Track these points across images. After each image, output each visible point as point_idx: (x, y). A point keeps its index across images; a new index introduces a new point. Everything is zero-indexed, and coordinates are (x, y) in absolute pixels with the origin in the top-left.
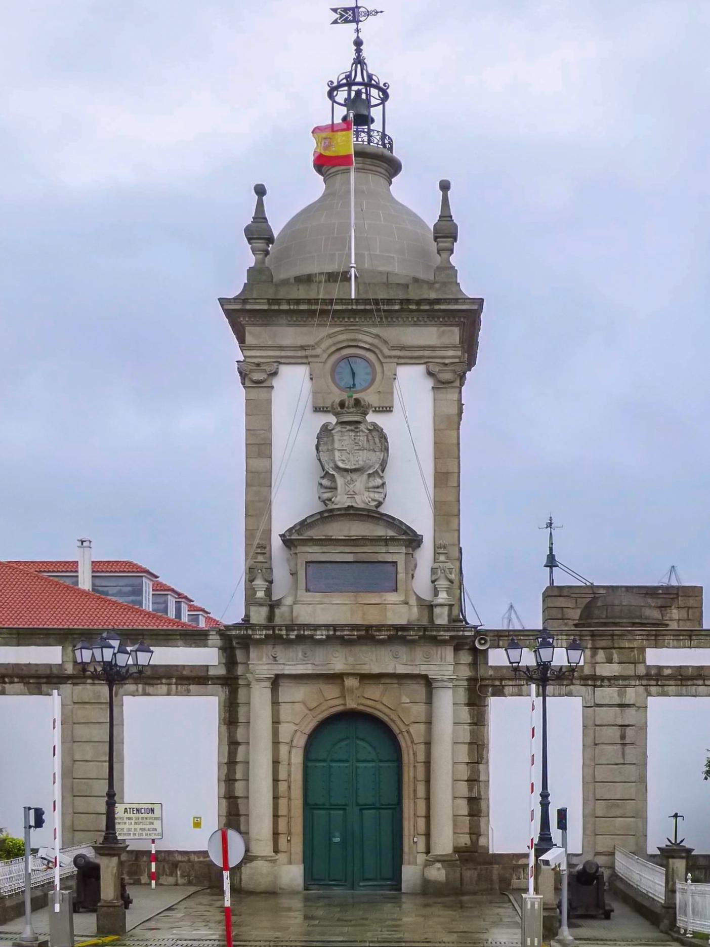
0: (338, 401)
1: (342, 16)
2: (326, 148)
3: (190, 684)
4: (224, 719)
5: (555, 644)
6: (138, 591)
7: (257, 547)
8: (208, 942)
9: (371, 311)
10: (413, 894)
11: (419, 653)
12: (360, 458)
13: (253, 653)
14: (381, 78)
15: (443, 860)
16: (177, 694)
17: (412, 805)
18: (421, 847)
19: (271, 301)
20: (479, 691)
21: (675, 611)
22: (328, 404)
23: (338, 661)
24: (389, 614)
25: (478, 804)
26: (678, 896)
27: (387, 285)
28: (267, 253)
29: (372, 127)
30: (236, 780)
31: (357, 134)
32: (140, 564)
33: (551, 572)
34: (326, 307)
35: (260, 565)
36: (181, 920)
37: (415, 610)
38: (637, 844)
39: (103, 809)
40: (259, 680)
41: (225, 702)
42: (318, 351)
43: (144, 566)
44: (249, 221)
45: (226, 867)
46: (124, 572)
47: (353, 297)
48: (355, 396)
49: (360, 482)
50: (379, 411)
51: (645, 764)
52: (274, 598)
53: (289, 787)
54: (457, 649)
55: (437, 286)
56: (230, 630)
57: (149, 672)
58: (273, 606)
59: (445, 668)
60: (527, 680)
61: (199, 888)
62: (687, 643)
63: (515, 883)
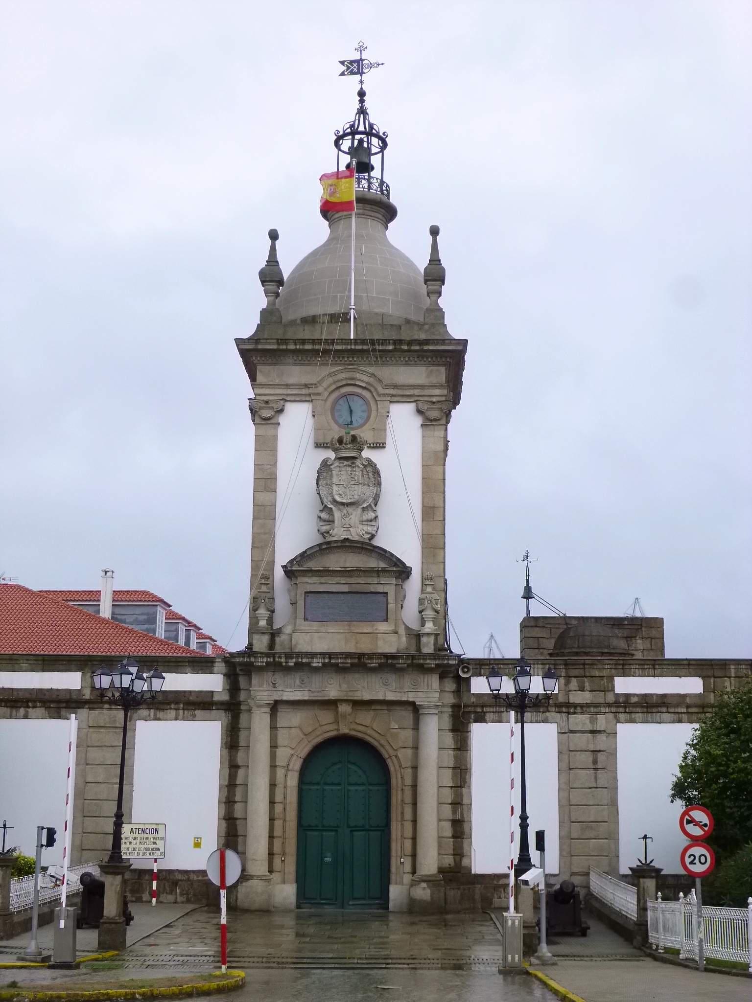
0: (337, 437)
1: (348, 68)
2: (332, 194)
4: (226, 743)
5: (532, 672)
6: (152, 620)
7: (261, 578)
8: (203, 958)
9: (367, 351)
10: (401, 912)
11: (407, 680)
12: (356, 492)
13: (255, 680)
14: (381, 127)
15: (428, 880)
17: (399, 826)
18: (408, 867)
19: (280, 341)
20: (463, 716)
21: (639, 641)
22: (328, 440)
23: (333, 687)
24: (380, 643)
25: (461, 826)
26: (650, 913)
27: (383, 326)
28: (277, 295)
29: (372, 174)
30: (235, 802)
31: (359, 181)
32: (155, 594)
33: (528, 603)
34: (328, 347)
35: (263, 595)
36: (179, 936)
37: (404, 639)
38: (610, 865)
39: (110, 828)
40: (260, 706)
42: (320, 389)
43: (159, 596)
44: (263, 264)
45: (223, 885)
46: (141, 601)
47: (352, 337)
48: (352, 433)
49: (355, 515)
50: (373, 447)
51: (616, 788)
52: (275, 627)
53: (285, 809)
54: (442, 677)
55: (426, 327)
56: (235, 657)
57: (160, 698)
58: (274, 635)
59: (431, 695)
60: (506, 707)
61: (197, 906)
62: (651, 672)
63: (496, 902)
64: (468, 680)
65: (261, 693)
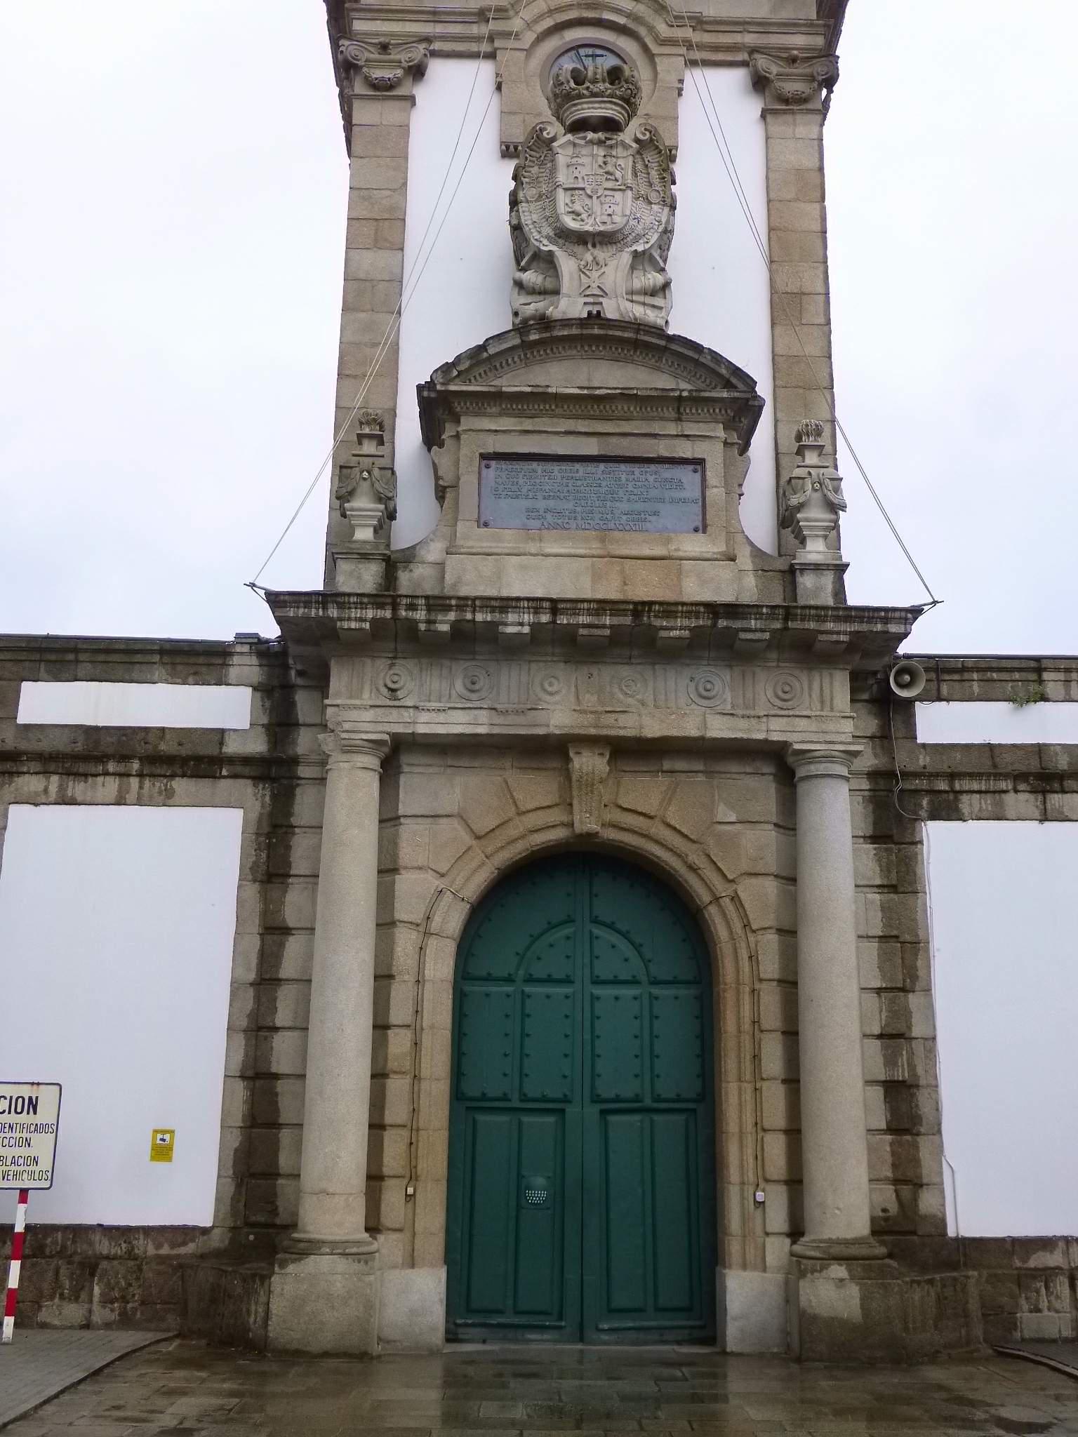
3: (173, 776)
7: (362, 434)
10: (759, 1358)
11: (764, 686)
12: (618, 209)
16: (139, 802)
17: (748, 1096)
18: (778, 1218)
30: (276, 1029)
40: (349, 749)
41: (260, 821)
42: (516, 24)
49: (614, 270)
58: (393, 564)
59: (831, 726)
64: (907, 707)
65: (354, 715)
